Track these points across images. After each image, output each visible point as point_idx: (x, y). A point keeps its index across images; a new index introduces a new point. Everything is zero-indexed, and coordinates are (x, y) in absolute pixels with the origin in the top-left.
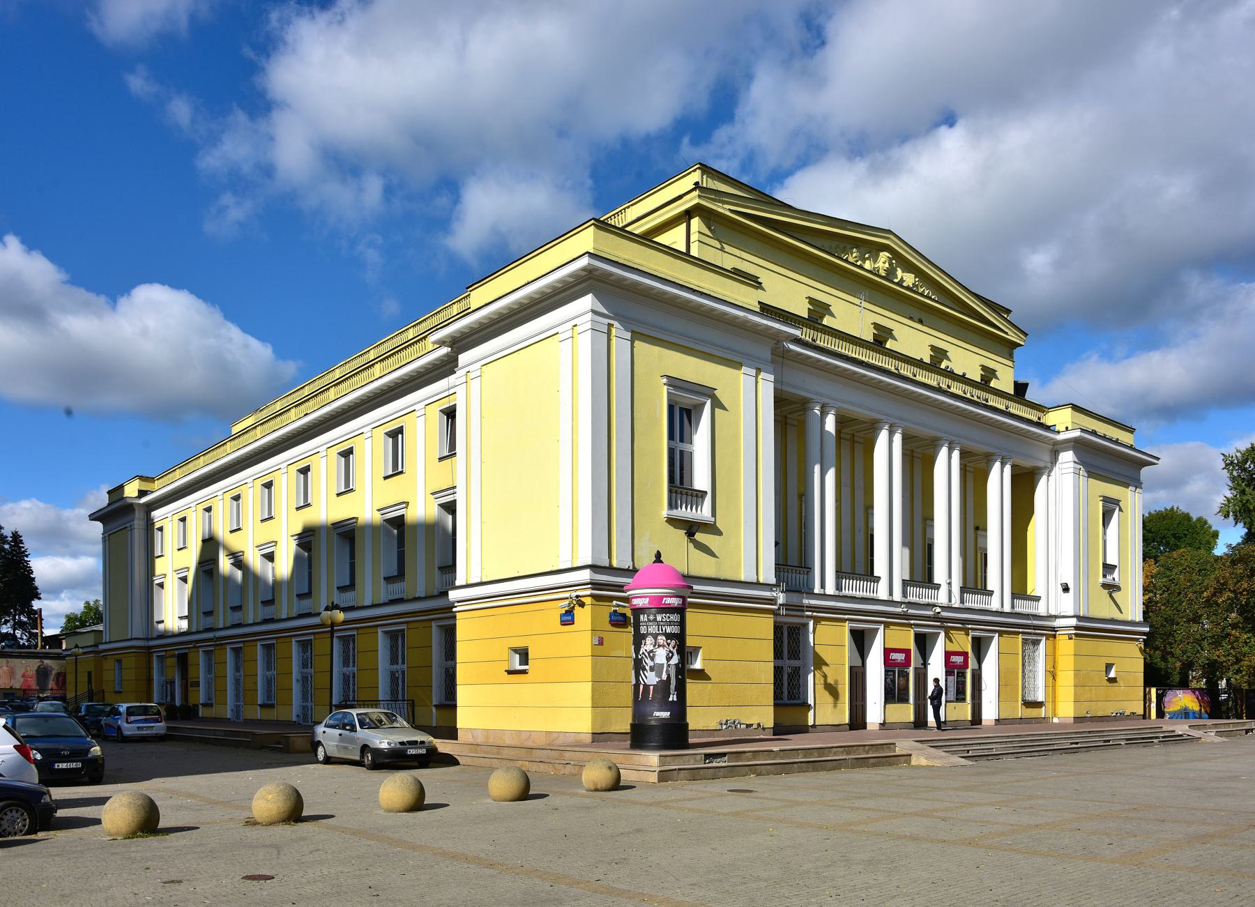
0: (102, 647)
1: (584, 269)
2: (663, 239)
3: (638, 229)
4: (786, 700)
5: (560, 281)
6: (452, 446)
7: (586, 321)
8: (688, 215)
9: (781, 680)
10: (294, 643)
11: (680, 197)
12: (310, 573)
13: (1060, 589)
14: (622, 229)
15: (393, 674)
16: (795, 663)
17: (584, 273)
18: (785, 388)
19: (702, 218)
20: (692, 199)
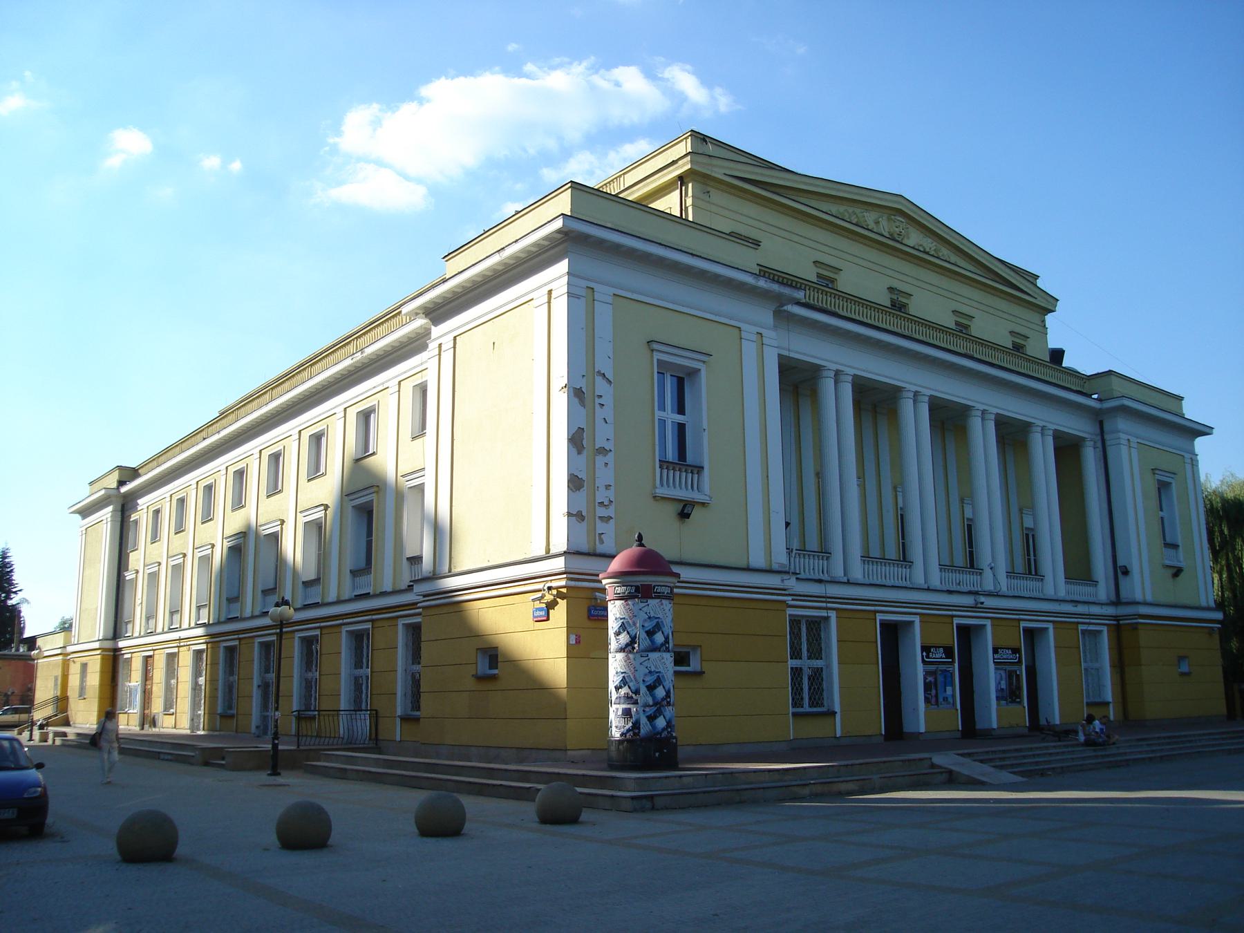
0: (70, 649)
1: (559, 231)
2: (660, 205)
3: (632, 196)
4: (806, 708)
5: (535, 244)
6: (423, 426)
7: (561, 287)
8: (682, 179)
9: (800, 683)
10: (400, 627)
11: (674, 162)
12: (1011, 539)
13: (149, 881)
14: (616, 196)
15: (356, 679)
16: (818, 663)
17: (559, 236)
18: (785, 353)
19: (693, 181)
20: (684, 165)
